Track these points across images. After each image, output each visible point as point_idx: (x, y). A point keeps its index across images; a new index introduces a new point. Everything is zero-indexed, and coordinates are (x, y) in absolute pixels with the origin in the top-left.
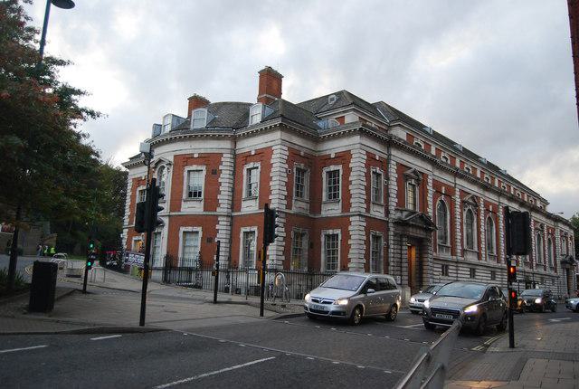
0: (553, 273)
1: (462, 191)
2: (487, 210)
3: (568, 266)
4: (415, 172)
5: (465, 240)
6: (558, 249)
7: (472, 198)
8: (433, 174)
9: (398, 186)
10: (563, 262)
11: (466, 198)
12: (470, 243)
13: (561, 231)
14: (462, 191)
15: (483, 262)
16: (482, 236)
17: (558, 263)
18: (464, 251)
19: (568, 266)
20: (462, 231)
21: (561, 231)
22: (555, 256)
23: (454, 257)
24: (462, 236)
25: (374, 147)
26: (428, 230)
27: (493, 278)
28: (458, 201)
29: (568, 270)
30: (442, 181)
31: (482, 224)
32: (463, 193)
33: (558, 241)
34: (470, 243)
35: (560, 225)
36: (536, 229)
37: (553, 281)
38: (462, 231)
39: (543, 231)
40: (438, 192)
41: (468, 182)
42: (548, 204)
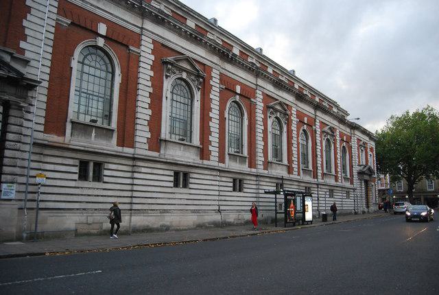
0: (348, 184)
1: (321, 123)
2: (342, 140)
3: (366, 177)
4: (281, 104)
5: (325, 165)
6: (355, 159)
7: (330, 128)
8: (297, 107)
9: (220, 101)
10: (360, 173)
11: (326, 129)
12: (277, 153)
13: (359, 140)
14: (321, 123)
15: (339, 184)
16: (294, 149)
17: (356, 176)
18: (323, 175)
19: (366, 177)
20: (322, 157)
21: (359, 140)
22: (351, 167)
23: (253, 170)
24: (322, 162)
25: (215, 61)
26: (370, 175)
27: (331, 196)
28: (318, 131)
29: (366, 182)
30: (305, 112)
31: (338, 152)
32: (323, 124)
33: (355, 150)
34: (277, 153)
35: (357, 133)
36: (323, 132)
37: (348, 193)
38: (322, 157)
39: (333, 136)
40: (301, 122)
41: (180, 35)
42: (348, 115)
